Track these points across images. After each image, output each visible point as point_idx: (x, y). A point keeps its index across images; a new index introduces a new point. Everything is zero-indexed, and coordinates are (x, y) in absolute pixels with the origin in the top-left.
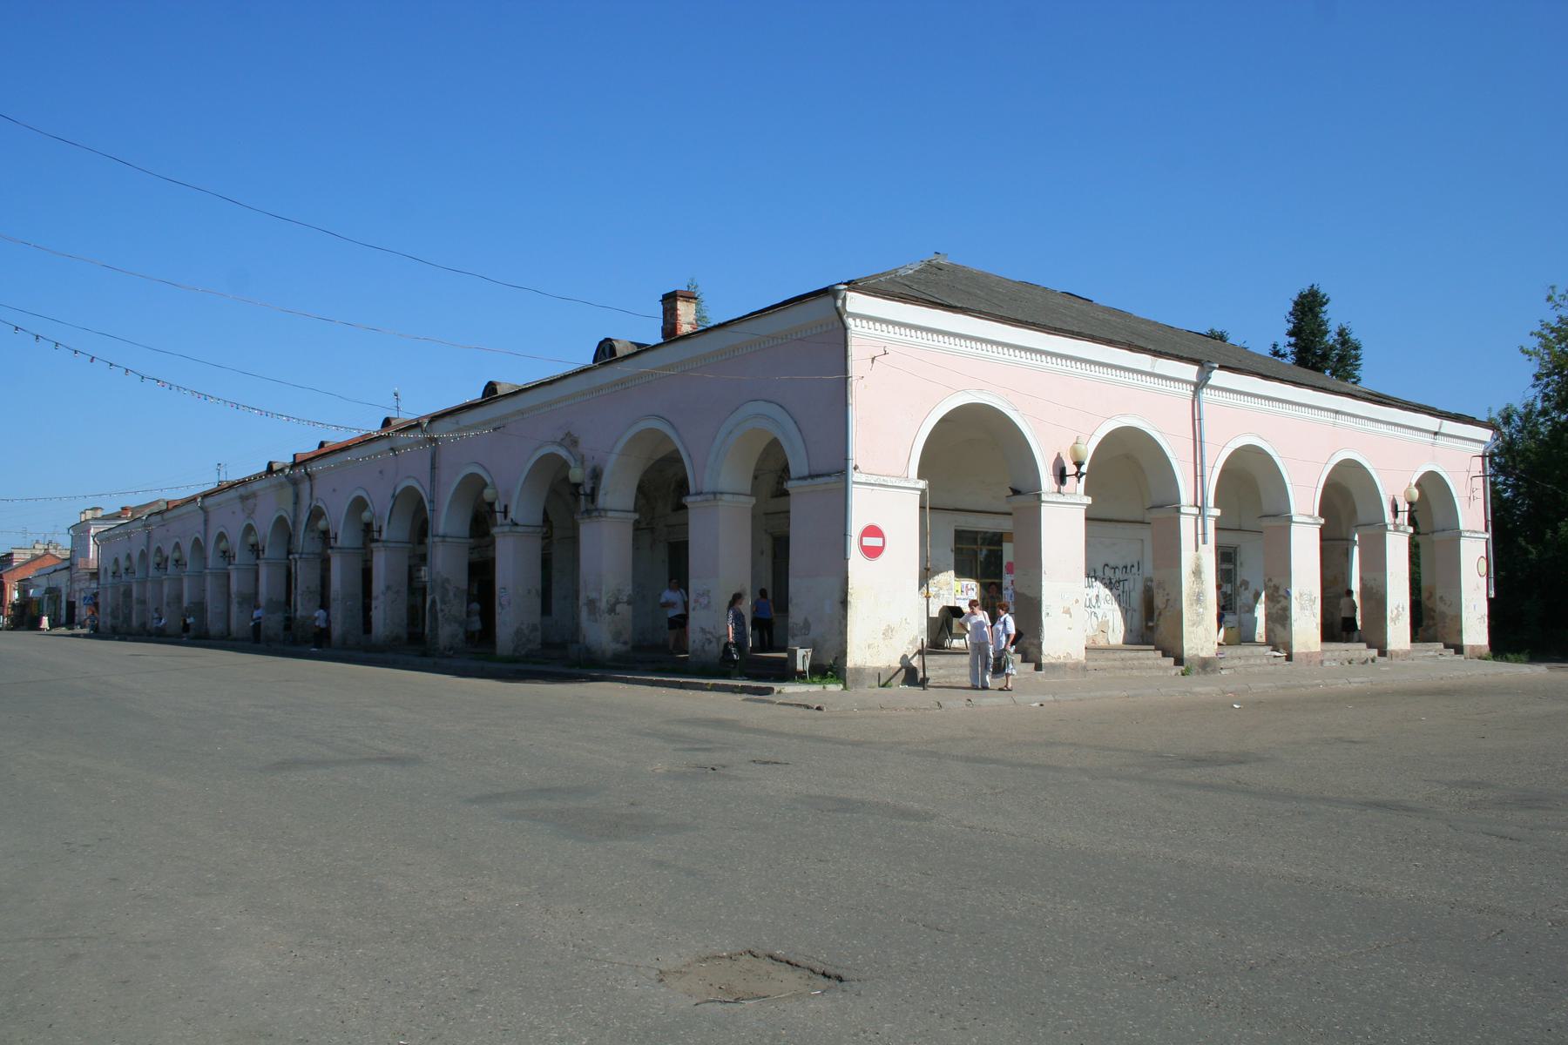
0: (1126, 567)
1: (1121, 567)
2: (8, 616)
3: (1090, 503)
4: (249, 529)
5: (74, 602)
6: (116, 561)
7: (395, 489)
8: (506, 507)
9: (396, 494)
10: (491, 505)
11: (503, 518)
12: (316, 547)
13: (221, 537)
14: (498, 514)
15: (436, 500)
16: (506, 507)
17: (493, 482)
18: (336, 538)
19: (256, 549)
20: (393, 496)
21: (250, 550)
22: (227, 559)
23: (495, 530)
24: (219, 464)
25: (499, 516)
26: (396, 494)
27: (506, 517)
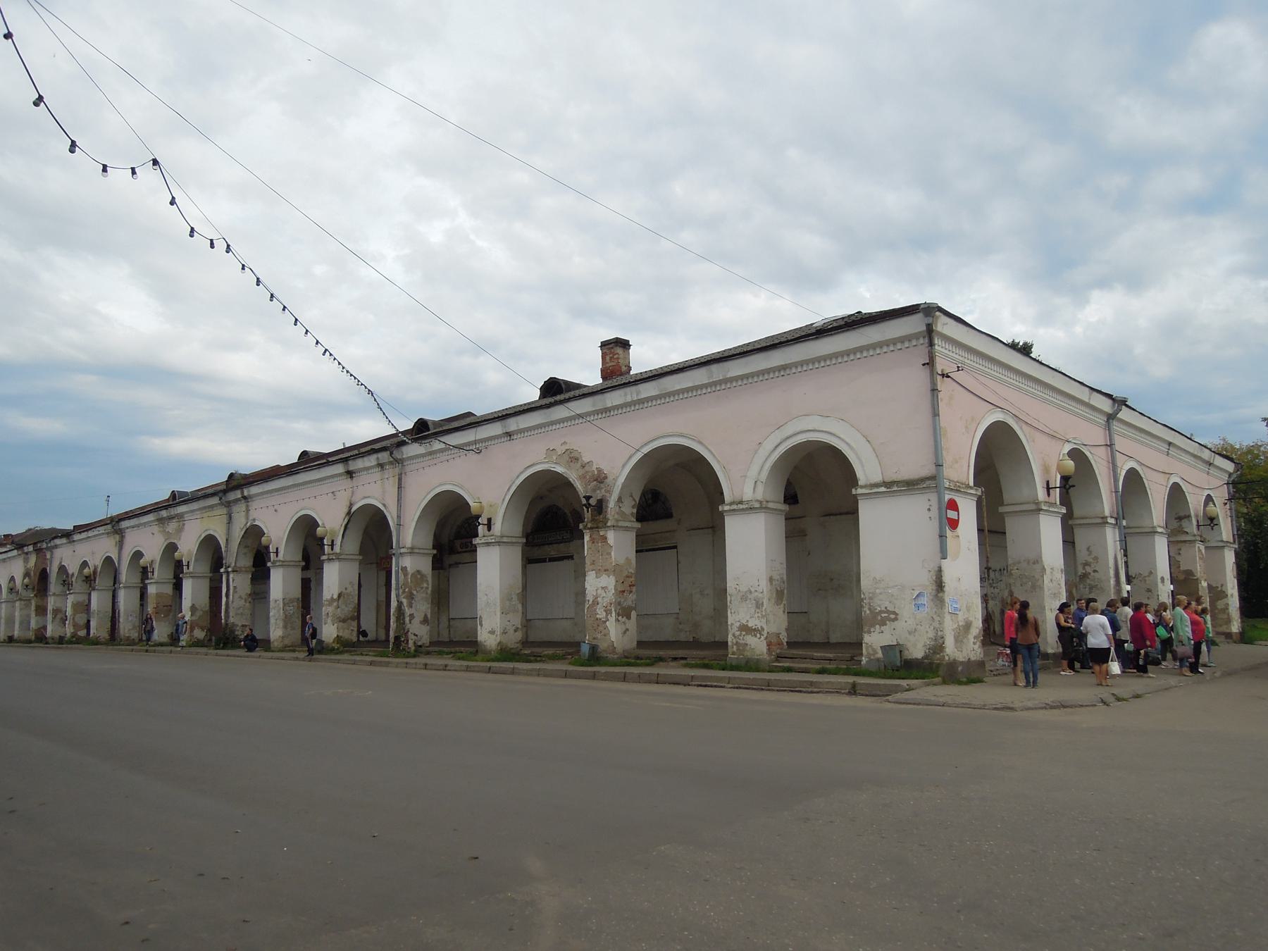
0: (1000, 570)
1: (998, 570)
2: (616, 570)
3: (1000, 508)
4: (171, 548)
5: (36, 616)
6: (12, 579)
7: (351, 505)
8: (277, 549)
9: (353, 510)
10: (267, 548)
11: (330, 549)
12: (136, 580)
13: (138, 555)
14: (326, 546)
15: (402, 516)
16: (277, 549)
17: (323, 524)
18: (277, 553)
19: (145, 572)
20: (349, 513)
21: (84, 581)
22: (89, 582)
23: (269, 564)
24: (108, 496)
25: (272, 556)
26: (353, 510)
27: (332, 549)
